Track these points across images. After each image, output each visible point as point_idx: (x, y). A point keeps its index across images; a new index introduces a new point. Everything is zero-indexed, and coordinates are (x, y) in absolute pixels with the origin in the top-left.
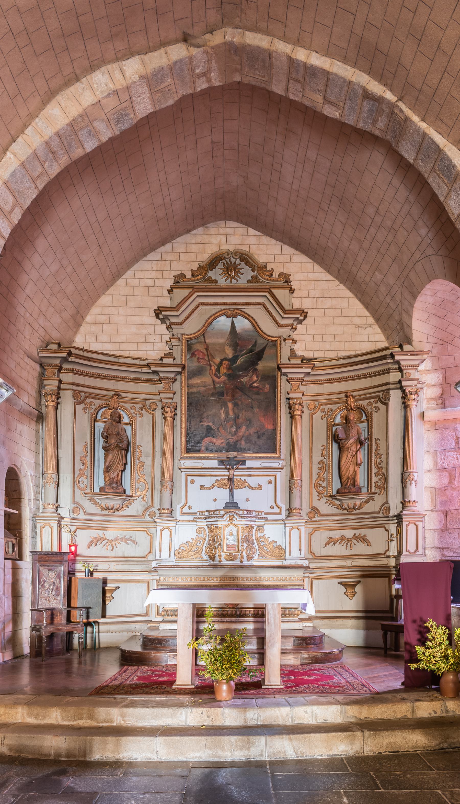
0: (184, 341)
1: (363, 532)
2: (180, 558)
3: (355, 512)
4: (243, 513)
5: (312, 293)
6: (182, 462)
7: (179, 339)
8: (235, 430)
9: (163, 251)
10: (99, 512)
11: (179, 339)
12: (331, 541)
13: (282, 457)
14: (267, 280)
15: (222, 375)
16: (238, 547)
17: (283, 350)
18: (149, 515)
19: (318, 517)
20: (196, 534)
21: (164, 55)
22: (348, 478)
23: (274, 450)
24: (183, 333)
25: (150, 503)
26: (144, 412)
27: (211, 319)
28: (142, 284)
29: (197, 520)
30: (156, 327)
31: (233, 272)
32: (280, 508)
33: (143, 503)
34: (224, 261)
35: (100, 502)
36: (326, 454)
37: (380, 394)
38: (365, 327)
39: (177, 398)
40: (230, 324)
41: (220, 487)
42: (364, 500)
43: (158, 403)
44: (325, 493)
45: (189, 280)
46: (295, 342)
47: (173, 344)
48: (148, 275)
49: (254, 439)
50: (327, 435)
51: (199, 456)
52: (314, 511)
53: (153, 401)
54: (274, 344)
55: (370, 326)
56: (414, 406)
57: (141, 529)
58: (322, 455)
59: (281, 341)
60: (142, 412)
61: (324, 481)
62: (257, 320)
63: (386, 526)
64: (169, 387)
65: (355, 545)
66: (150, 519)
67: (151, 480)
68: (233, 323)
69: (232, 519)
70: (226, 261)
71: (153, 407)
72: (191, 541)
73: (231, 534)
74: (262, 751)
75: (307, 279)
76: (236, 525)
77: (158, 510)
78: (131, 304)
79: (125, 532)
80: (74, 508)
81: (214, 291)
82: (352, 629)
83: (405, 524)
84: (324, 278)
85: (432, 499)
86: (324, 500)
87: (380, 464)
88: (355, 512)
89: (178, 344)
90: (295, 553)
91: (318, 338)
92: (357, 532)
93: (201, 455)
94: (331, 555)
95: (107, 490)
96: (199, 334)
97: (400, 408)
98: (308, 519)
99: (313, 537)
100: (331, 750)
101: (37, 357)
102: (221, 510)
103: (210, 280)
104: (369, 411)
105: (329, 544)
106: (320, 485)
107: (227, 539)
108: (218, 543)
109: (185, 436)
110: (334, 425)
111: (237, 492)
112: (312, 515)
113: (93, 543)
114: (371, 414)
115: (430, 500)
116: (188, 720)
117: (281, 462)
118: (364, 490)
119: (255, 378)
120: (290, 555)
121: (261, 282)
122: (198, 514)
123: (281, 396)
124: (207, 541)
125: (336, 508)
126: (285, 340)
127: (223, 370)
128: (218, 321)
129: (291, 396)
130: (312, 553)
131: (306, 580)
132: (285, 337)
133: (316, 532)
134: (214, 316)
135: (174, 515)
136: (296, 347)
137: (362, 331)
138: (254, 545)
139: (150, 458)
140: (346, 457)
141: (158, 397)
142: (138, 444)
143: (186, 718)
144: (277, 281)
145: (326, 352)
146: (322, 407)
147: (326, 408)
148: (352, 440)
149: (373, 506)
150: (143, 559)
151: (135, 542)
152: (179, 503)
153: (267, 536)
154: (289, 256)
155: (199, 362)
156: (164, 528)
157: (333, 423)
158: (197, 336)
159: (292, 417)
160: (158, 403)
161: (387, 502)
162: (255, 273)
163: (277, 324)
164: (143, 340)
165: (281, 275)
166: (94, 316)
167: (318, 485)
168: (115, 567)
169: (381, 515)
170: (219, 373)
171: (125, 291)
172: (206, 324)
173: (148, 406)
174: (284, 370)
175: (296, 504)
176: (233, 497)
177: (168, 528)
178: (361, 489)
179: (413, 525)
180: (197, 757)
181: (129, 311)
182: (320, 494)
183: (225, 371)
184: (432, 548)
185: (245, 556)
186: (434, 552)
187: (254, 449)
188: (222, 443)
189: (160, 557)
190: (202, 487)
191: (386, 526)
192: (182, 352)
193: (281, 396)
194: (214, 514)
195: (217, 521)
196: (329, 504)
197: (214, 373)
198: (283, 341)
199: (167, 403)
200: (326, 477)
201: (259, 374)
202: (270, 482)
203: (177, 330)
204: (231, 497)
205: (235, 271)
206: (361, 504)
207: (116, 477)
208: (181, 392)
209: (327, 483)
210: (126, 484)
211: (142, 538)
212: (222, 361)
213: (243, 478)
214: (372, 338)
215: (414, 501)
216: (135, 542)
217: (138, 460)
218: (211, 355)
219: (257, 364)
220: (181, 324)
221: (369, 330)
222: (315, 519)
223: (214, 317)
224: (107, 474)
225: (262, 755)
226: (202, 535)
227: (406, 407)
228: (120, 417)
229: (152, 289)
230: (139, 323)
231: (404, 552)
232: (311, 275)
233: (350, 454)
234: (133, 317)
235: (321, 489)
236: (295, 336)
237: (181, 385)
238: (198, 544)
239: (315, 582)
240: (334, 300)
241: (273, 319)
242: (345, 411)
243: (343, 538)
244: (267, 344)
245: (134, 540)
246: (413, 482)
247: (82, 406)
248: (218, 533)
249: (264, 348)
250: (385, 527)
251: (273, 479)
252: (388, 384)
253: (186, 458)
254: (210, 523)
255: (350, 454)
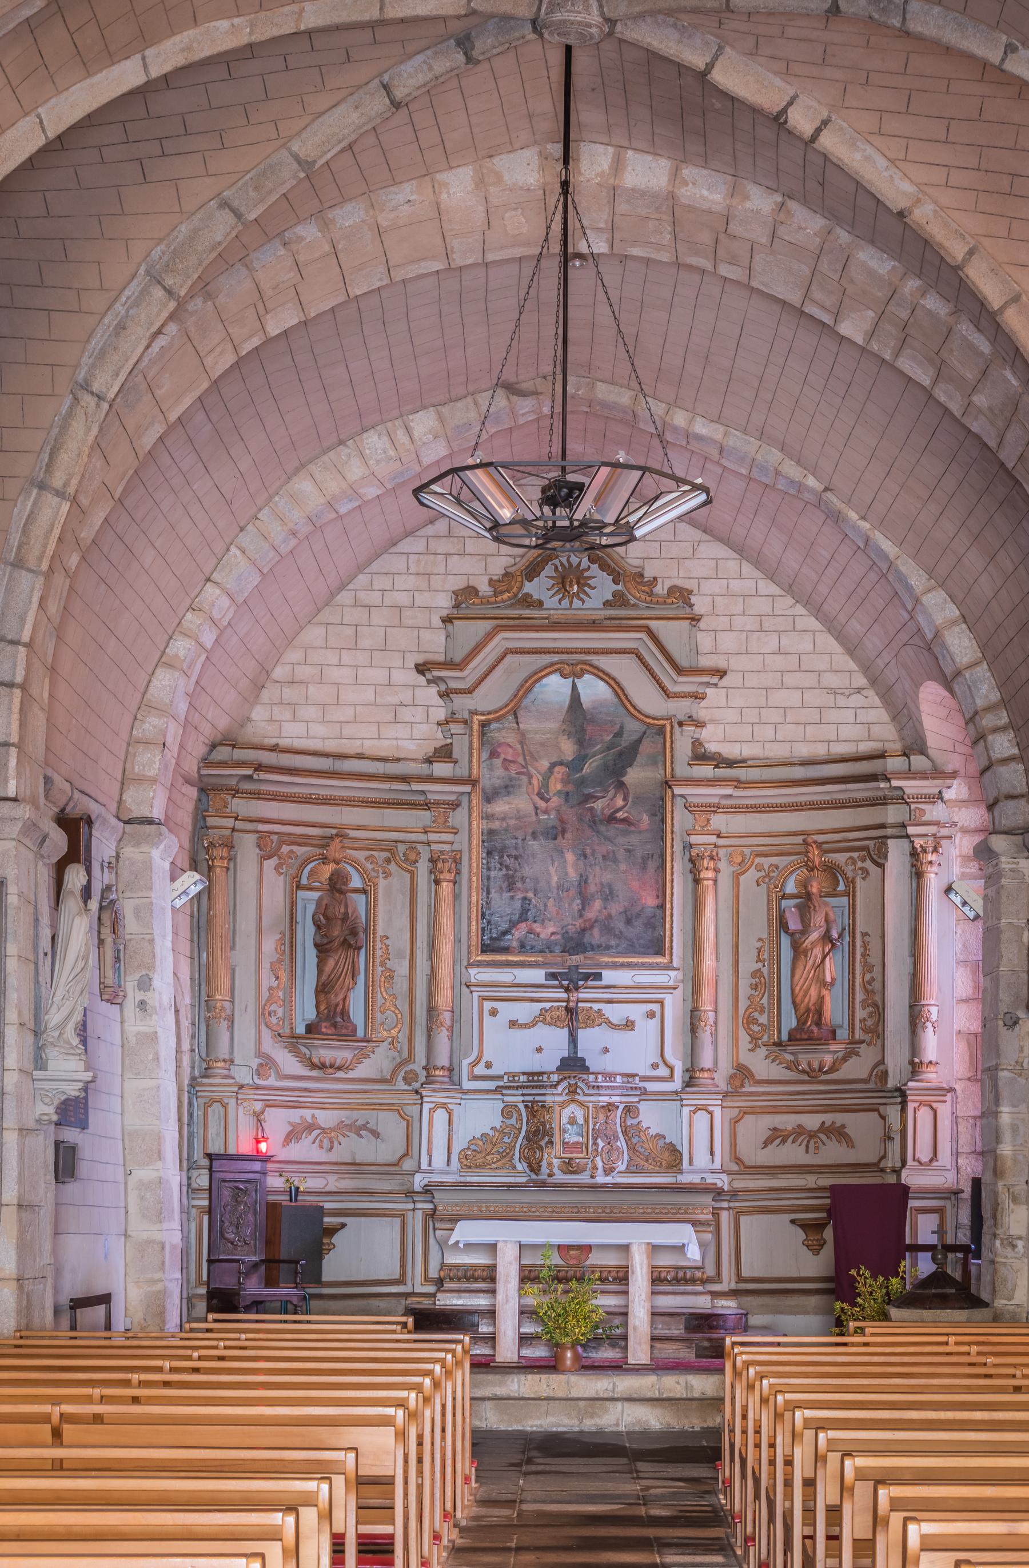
0: (475, 727)
1: (839, 1118)
2: (470, 1167)
3: (823, 1077)
4: (596, 1078)
5: (739, 622)
6: (473, 971)
7: (465, 722)
8: (580, 907)
9: (430, 534)
10: (306, 1072)
11: (465, 722)
12: (776, 1136)
13: (675, 964)
14: (645, 601)
15: (554, 795)
16: (587, 1148)
17: (677, 746)
18: (404, 1079)
19: (750, 1086)
20: (501, 1119)
21: (472, 405)
22: (808, 1010)
23: (660, 951)
24: (472, 708)
25: (405, 1054)
26: (393, 867)
27: (530, 682)
28: (387, 602)
29: (505, 1092)
30: (418, 691)
31: (576, 587)
32: (671, 1069)
33: (393, 1053)
34: (556, 562)
35: (308, 1053)
36: (766, 956)
37: (871, 843)
38: (847, 692)
39: (461, 841)
40: (568, 691)
41: (550, 1024)
42: (840, 1055)
43: (420, 848)
44: (765, 1038)
45: (485, 601)
46: (700, 724)
47: (453, 731)
48: (401, 582)
49: (619, 925)
50: (769, 919)
51: (507, 961)
52: (742, 1073)
53: (412, 845)
54: (659, 730)
55: (859, 690)
56: (933, 875)
57: (389, 1107)
58: (759, 960)
59: (672, 727)
60: (389, 867)
61: (762, 1011)
62: (625, 684)
63: (881, 1108)
64: (446, 821)
65: (824, 1144)
66: (406, 1087)
67: (407, 1007)
68: (574, 687)
69: (575, 1092)
70: (561, 562)
71: (412, 856)
72: (491, 1133)
73: (572, 1121)
74: (618, 1420)
75: (728, 593)
76: (581, 1104)
77: (424, 1068)
78: (365, 643)
79: (355, 1112)
80: (261, 1065)
81: (537, 631)
82: (816, 1314)
83: (911, 1106)
84: (763, 591)
85: (971, 1056)
86: (762, 1052)
87: (869, 983)
88: (823, 1077)
89: (462, 732)
90: (701, 1159)
91: (751, 715)
92: (828, 1118)
93: (510, 958)
94: (777, 1163)
95: (324, 1030)
96: (507, 713)
97: (907, 874)
98: (730, 1089)
99: (741, 1127)
100: (705, 1421)
101: (196, 775)
102: (553, 1073)
103: (527, 601)
104: (850, 875)
105: (772, 1142)
106: (755, 1021)
107: (565, 1131)
108: (547, 1139)
109: (477, 919)
110: (783, 897)
111: (584, 1035)
112: (738, 1083)
113: (293, 1135)
114: (853, 882)
115: (967, 1058)
116: (522, 1390)
117: (673, 974)
118: (842, 1034)
119: (620, 803)
120: (691, 1163)
121: (633, 605)
122: (506, 1080)
123: (672, 839)
124: (523, 1133)
125: (786, 1068)
126: (681, 724)
127: (556, 785)
128: (545, 685)
129: (694, 839)
130: (738, 1160)
131: (724, 1216)
132: (681, 717)
133: (746, 1116)
134: (536, 677)
135: (455, 1079)
136: (705, 734)
137: (841, 701)
138: (618, 1144)
139: (406, 963)
140: (802, 967)
141: (422, 837)
142: (380, 932)
143: (519, 1386)
144: (665, 603)
145: (767, 745)
146: (757, 860)
147: (766, 862)
148: (814, 936)
149: (857, 1068)
150: (392, 1168)
151: (375, 1134)
152: (466, 1057)
153: (645, 1125)
154: (689, 545)
155: (506, 769)
156: (438, 1106)
157: (780, 894)
158: (501, 716)
159: (697, 881)
160: (420, 848)
161: (882, 1062)
162: (619, 587)
163: (665, 692)
164: (390, 717)
165: (672, 590)
166: (288, 668)
167: (750, 1021)
168: (337, 1184)
169: (871, 1086)
170: (547, 792)
171: (353, 615)
172: (521, 693)
173: (401, 855)
174: (678, 790)
175: (706, 1059)
176: (576, 1047)
177: (444, 1106)
178: (834, 1032)
179: (927, 1109)
180: (536, 1426)
181: (362, 658)
182: (754, 1038)
183: (559, 787)
184: (969, 1153)
185: (600, 1165)
186: (973, 1162)
187: (617, 946)
188: (553, 934)
189: (430, 1165)
190: (513, 1024)
191: (881, 1108)
192: (471, 748)
193: (672, 839)
194: (539, 1081)
195: (544, 1095)
196: (773, 1061)
197: (536, 791)
198: (676, 726)
199: (441, 852)
200: (766, 1005)
201: (628, 793)
202: (651, 1015)
203: (463, 704)
204: (572, 1046)
205: (578, 583)
206: (834, 1063)
207: (341, 1003)
208: (470, 830)
209: (769, 1017)
210: (357, 1013)
211: (391, 1125)
212: (553, 765)
213: (596, 1006)
214: (863, 716)
215: (931, 1062)
216: (375, 1134)
217: (381, 965)
218: (531, 754)
219: (624, 774)
220: (469, 692)
221: (856, 700)
222: (744, 1090)
223: (537, 676)
224: (322, 997)
225: (617, 1425)
226: (513, 1121)
227: (918, 875)
228: (346, 879)
229: (407, 613)
230: (382, 682)
231: (910, 1162)
232: (736, 585)
233: (811, 962)
234: (368, 670)
235: (756, 1028)
236: (701, 710)
237: (470, 816)
238: (506, 1139)
239: (744, 1220)
240: (783, 636)
241: (657, 681)
242: (805, 871)
243: (800, 1131)
244: (645, 733)
245: (374, 1128)
246: (929, 1025)
247: (273, 862)
248: (547, 1118)
249: (639, 741)
250: (877, 1110)
251: (656, 1007)
252: (883, 826)
253: (479, 965)
254: (530, 1098)
255: (811, 962)
